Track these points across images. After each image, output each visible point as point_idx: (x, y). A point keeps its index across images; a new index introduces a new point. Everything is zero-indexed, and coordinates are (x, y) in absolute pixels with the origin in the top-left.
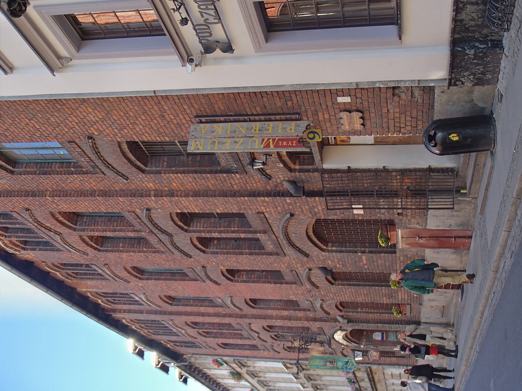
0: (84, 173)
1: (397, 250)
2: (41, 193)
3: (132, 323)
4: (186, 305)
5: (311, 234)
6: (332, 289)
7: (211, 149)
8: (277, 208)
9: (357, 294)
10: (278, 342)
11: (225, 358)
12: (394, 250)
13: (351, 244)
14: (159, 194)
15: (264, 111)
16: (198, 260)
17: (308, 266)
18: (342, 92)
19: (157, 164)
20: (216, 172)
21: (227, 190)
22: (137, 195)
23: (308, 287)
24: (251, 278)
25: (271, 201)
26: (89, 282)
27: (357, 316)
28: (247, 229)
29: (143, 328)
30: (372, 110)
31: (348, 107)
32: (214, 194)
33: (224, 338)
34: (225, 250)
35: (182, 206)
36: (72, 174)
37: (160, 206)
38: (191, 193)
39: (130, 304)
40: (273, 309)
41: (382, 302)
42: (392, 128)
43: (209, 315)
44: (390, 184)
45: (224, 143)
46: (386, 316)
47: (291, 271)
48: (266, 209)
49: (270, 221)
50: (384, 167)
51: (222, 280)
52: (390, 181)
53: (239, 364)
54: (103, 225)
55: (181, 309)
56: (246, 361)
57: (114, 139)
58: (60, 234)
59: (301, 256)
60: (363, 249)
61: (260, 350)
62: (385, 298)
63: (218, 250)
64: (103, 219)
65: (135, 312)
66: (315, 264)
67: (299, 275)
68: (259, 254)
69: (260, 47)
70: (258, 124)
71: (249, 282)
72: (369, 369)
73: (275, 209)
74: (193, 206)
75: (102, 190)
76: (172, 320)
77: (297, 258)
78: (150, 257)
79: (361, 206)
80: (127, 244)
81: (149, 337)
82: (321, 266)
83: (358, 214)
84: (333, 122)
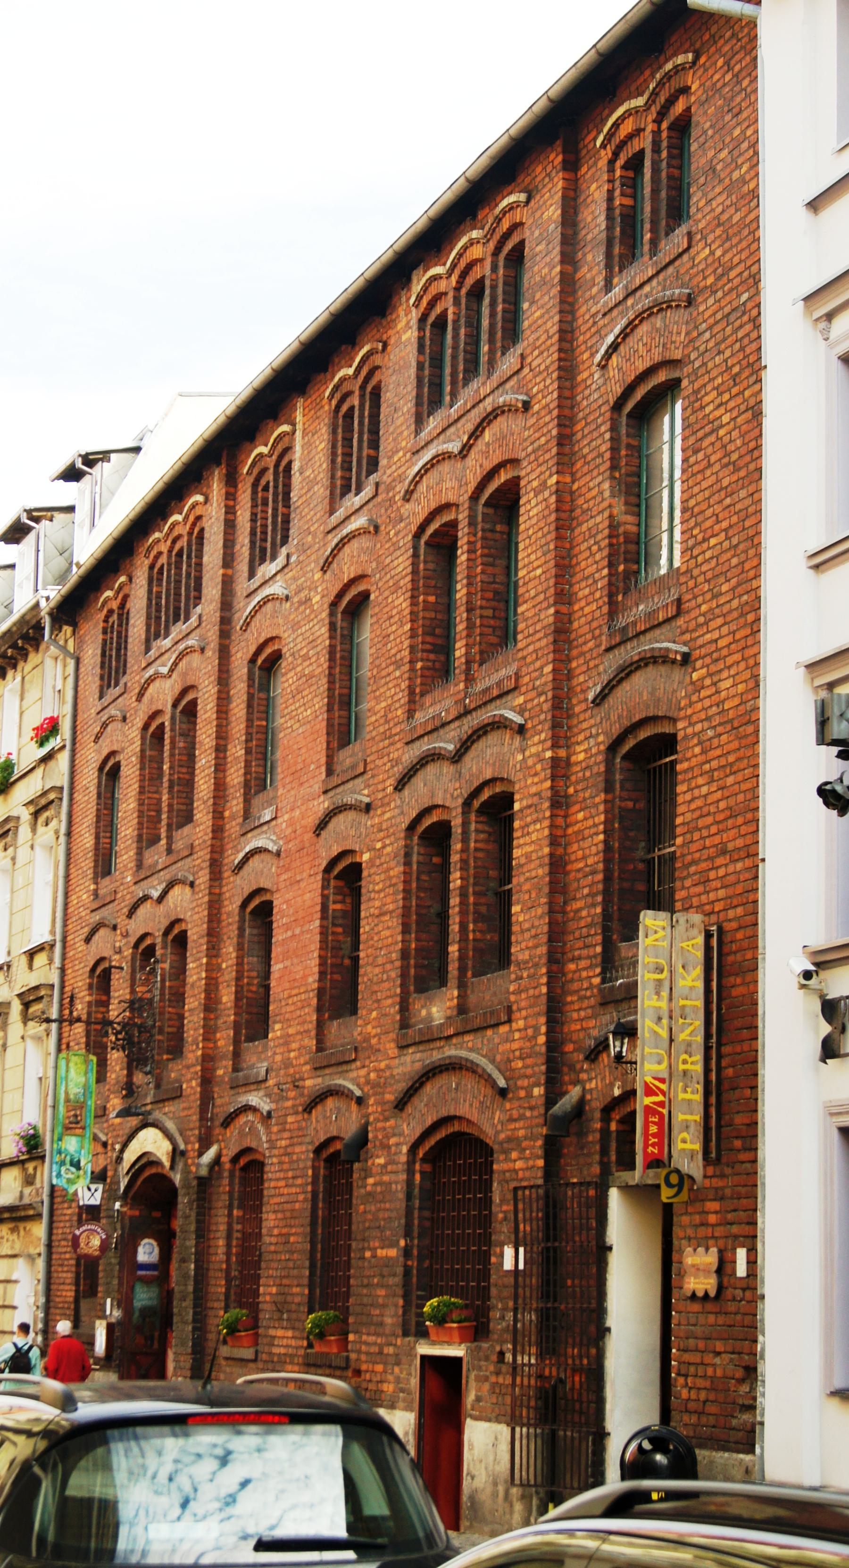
0: (611, 595)
1: (411, 1339)
2: (566, 459)
3: (192, 518)
4: (249, 706)
5: (456, 1127)
6: (304, 1148)
7: (645, 966)
8: (521, 1058)
9: (288, 1214)
10: (128, 952)
11: (63, 760)
12: (413, 1329)
13: (428, 1224)
14: (559, 769)
15: (726, 1085)
16: (389, 804)
17: (371, 1101)
18: (752, 1262)
19: (628, 785)
20: (606, 930)
21: (565, 944)
22: (558, 713)
23: (309, 1083)
24: (334, 925)
25: (537, 1048)
26: (322, 444)
27: (220, 1204)
28: (470, 963)
29: (174, 542)
30: (721, 1320)
31: (728, 1268)
32: (557, 908)
33: (142, 787)
34: (414, 885)
35: (529, 819)
36: (611, 565)
37: (530, 762)
38: (560, 851)
39: (253, 533)
40: (240, 963)
41: (262, 1281)
42: (686, 1357)
43: (220, 767)
44: (570, 1341)
45: (658, 993)
46: (218, 1287)
47: (356, 1049)
48: (519, 1030)
49: (489, 1032)
50: (609, 1330)
51: (329, 847)
52: (578, 1340)
53: (43, 802)
54: (485, 578)
55: (239, 689)
56: (53, 824)
57: (682, 714)
58: (465, 451)
59: (402, 1086)
60: (415, 1252)
61: (96, 883)
62: (274, 1290)
63: (415, 867)
64: (501, 578)
65: (229, 543)
66: (377, 1120)
67: (344, 1067)
68: (404, 975)
69: (832, 1114)
70: (699, 1068)
71: (324, 917)
72: (31, 1212)
73: (517, 1053)
74: (528, 849)
75: (570, 622)
76: (202, 650)
77: (392, 1076)
78: (398, 673)
79: (521, 1266)
80: (433, 615)
81: (142, 550)
82: (370, 1135)
83: (502, 1255)
84: (702, 1232)
